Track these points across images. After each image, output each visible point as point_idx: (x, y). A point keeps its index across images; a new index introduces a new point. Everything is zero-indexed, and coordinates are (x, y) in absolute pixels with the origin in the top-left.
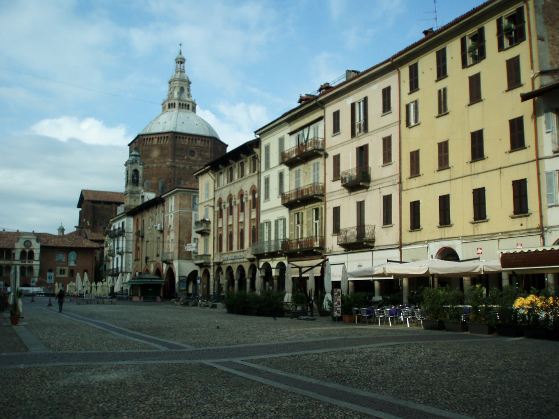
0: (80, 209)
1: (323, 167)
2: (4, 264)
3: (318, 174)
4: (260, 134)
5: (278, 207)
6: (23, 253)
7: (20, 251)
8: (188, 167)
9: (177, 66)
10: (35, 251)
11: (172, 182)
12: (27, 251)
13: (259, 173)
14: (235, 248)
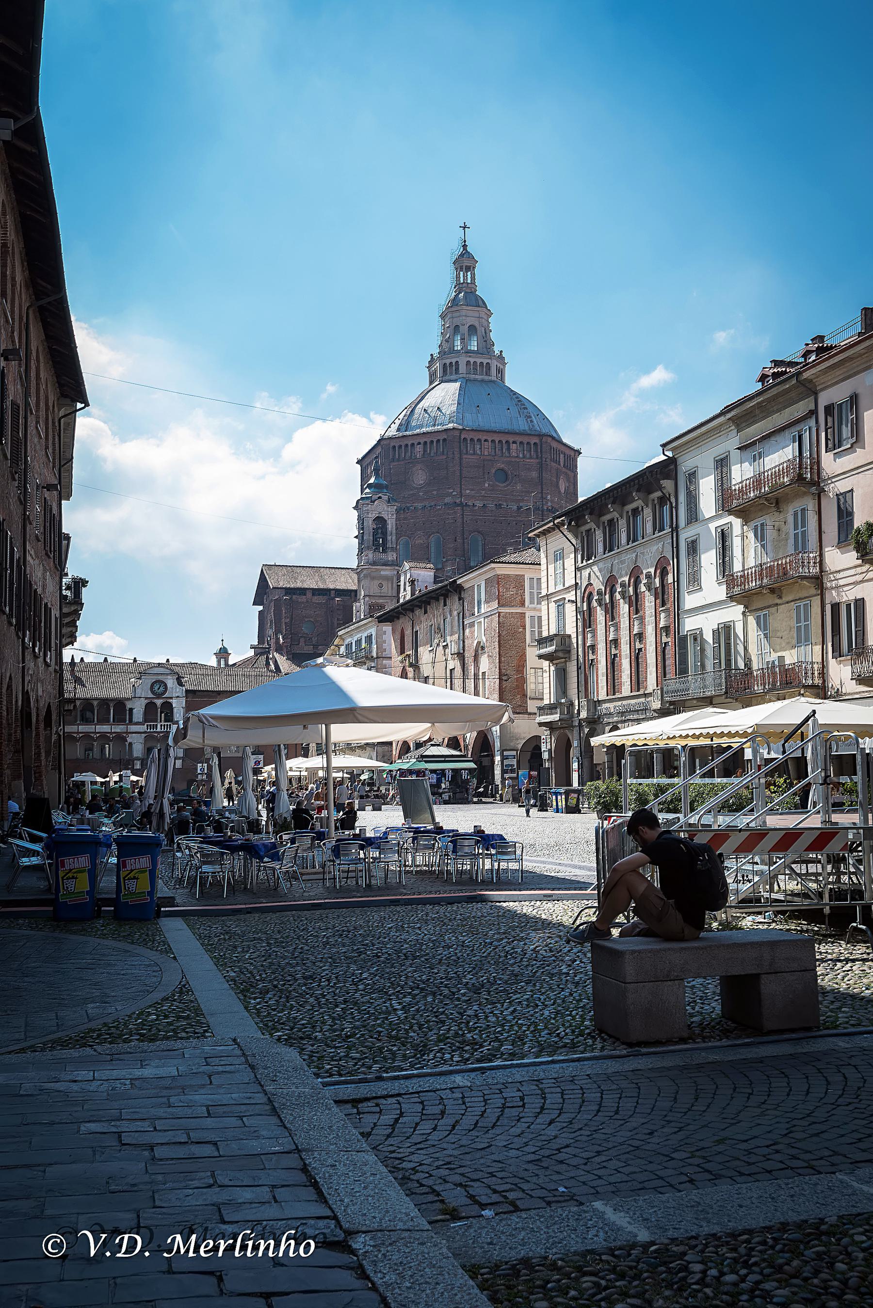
0: (261, 608)
1: (816, 517)
2: (111, 733)
3: (803, 533)
4: (672, 450)
5: (720, 603)
6: (150, 708)
7: (144, 702)
8: (491, 506)
9: (458, 277)
10: (174, 703)
11: (459, 540)
12: (159, 702)
13: (675, 530)
14: (626, 690)
